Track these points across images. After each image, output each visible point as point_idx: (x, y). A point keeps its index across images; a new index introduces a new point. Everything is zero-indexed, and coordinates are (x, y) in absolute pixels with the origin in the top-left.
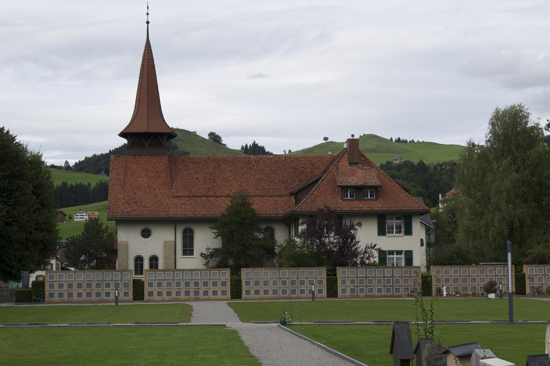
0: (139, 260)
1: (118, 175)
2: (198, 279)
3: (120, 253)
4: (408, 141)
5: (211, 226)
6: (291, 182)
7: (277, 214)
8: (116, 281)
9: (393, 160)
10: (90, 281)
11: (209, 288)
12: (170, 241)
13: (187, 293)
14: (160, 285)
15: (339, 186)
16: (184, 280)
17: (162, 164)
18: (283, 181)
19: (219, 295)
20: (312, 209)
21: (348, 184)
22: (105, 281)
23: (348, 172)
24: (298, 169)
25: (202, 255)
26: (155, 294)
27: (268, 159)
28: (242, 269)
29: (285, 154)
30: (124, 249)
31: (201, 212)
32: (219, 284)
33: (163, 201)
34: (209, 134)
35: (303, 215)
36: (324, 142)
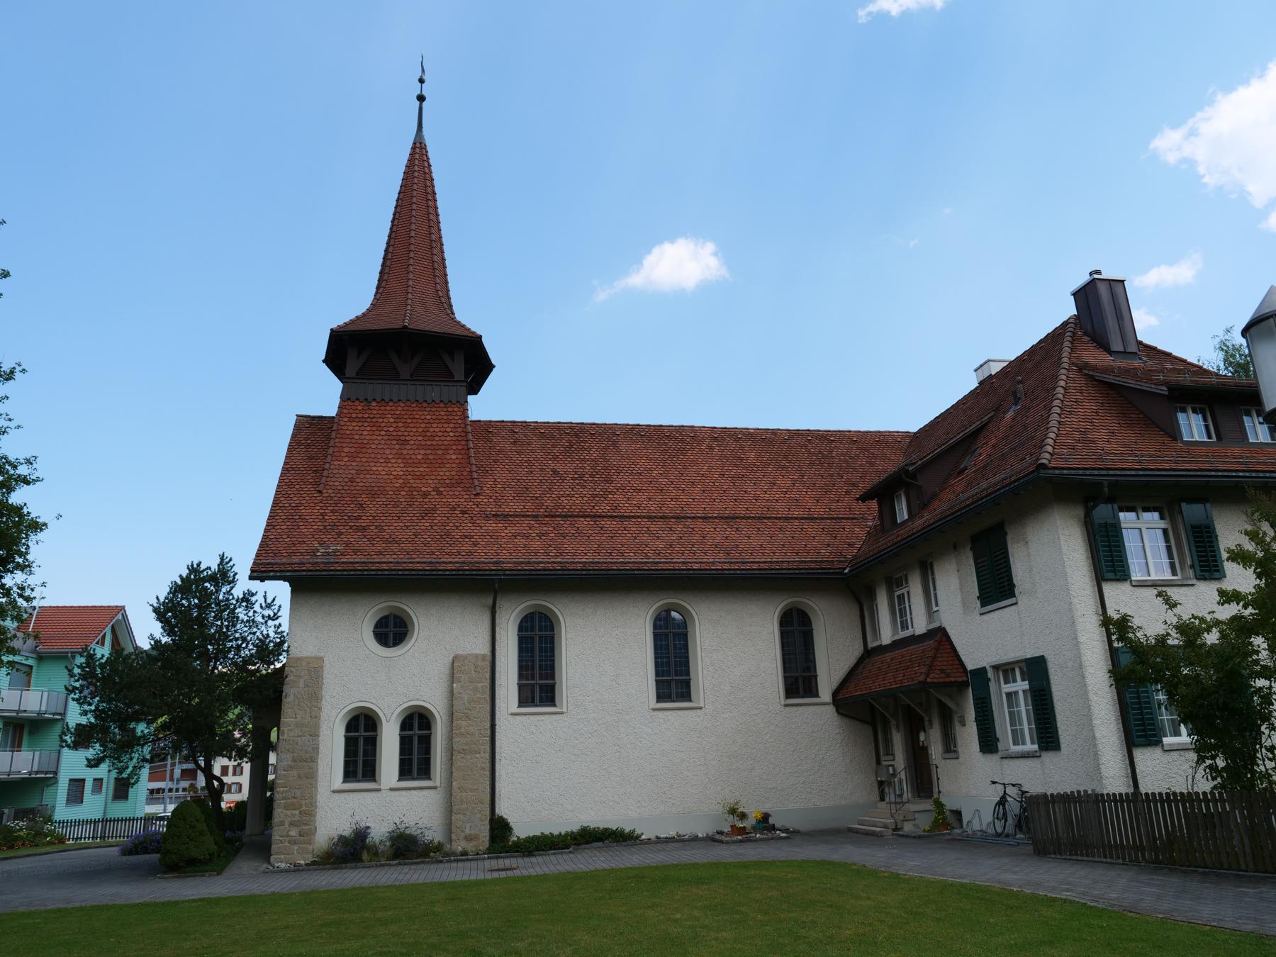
12: (477, 656)
17: (452, 425)
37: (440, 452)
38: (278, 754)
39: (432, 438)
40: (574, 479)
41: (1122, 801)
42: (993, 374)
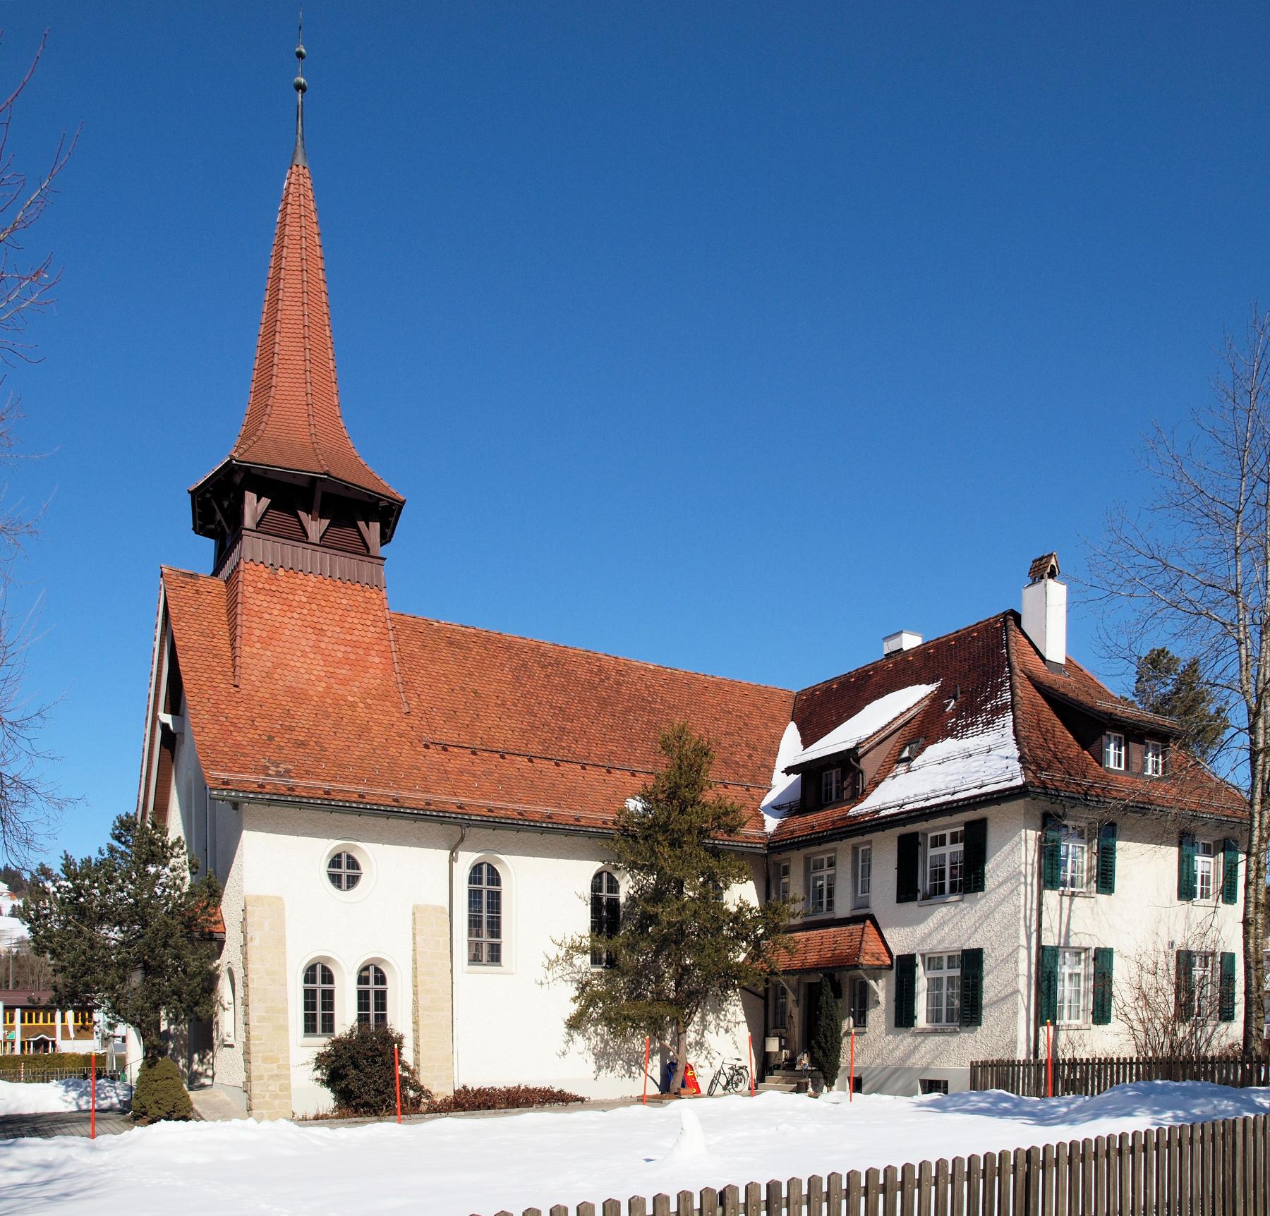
17: (371, 617)
37: (361, 652)
39: (351, 632)
41: (1131, 1063)
42: (905, 649)
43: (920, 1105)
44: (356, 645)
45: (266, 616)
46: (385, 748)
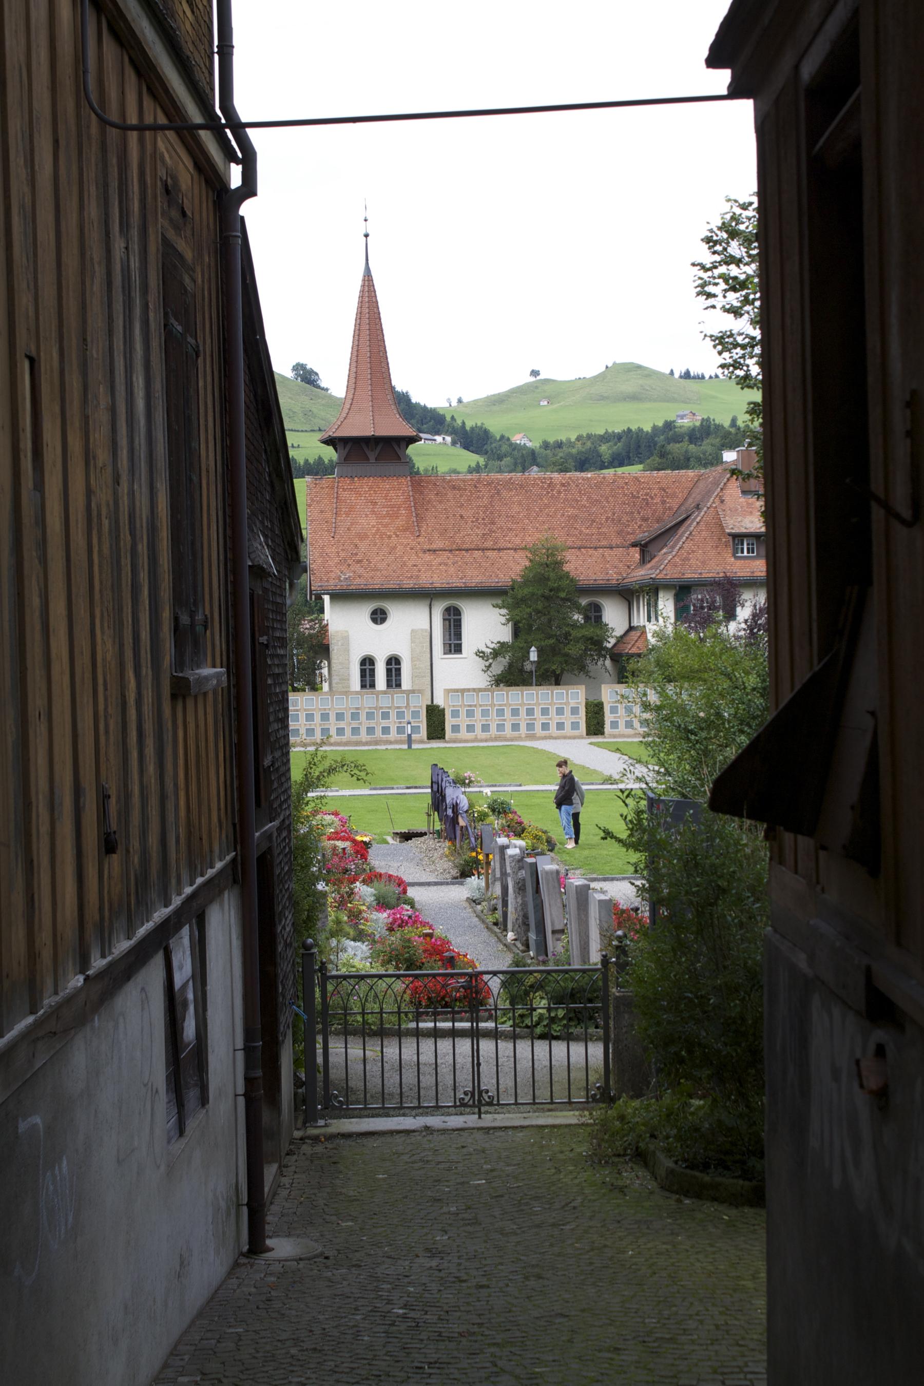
0: (367, 664)
1: (322, 512)
2: (533, 705)
3: (335, 651)
4: (707, 377)
5: (495, 602)
6: (628, 521)
7: (608, 580)
8: (398, 708)
9: (678, 416)
10: (357, 709)
11: (550, 719)
12: (422, 630)
13: (515, 727)
14: (470, 714)
15: (730, 534)
16: (510, 705)
18: (613, 520)
19: (568, 730)
20: (683, 574)
21: (744, 531)
22: (381, 708)
23: (741, 507)
24: (638, 497)
25: (480, 654)
26: (463, 729)
27: (583, 479)
28: (603, 686)
29: (450, 405)
30: (342, 645)
31: (475, 578)
32: (567, 711)
33: (405, 559)
34: (294, 367)
35: (667, 586)
36: (532, 379)
37: (395, 509)
38: (485, 690)
40: (472, 522)
43: (591, 744)
44: (392, 507)
45: (348, 501)
46: (402, 557)
